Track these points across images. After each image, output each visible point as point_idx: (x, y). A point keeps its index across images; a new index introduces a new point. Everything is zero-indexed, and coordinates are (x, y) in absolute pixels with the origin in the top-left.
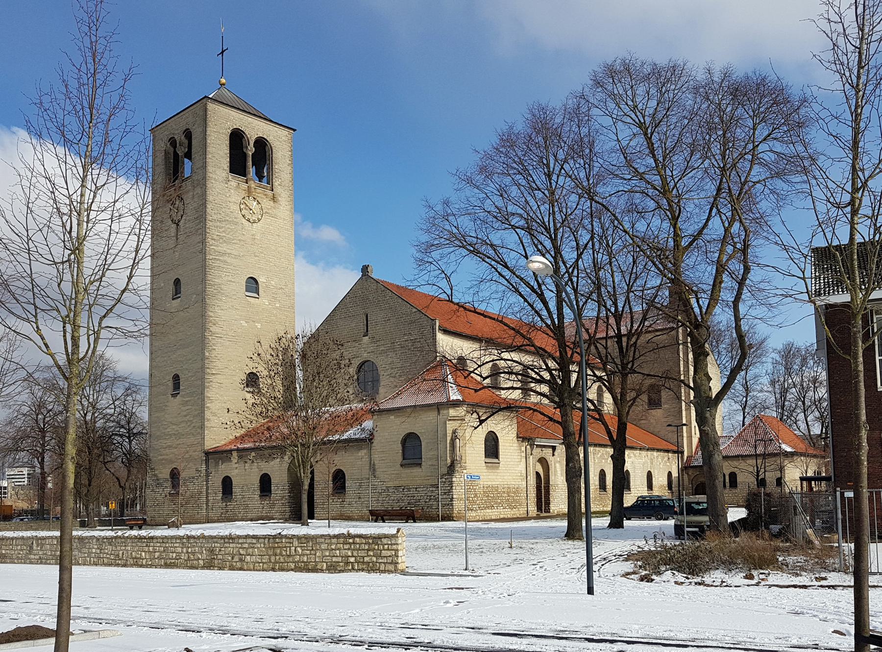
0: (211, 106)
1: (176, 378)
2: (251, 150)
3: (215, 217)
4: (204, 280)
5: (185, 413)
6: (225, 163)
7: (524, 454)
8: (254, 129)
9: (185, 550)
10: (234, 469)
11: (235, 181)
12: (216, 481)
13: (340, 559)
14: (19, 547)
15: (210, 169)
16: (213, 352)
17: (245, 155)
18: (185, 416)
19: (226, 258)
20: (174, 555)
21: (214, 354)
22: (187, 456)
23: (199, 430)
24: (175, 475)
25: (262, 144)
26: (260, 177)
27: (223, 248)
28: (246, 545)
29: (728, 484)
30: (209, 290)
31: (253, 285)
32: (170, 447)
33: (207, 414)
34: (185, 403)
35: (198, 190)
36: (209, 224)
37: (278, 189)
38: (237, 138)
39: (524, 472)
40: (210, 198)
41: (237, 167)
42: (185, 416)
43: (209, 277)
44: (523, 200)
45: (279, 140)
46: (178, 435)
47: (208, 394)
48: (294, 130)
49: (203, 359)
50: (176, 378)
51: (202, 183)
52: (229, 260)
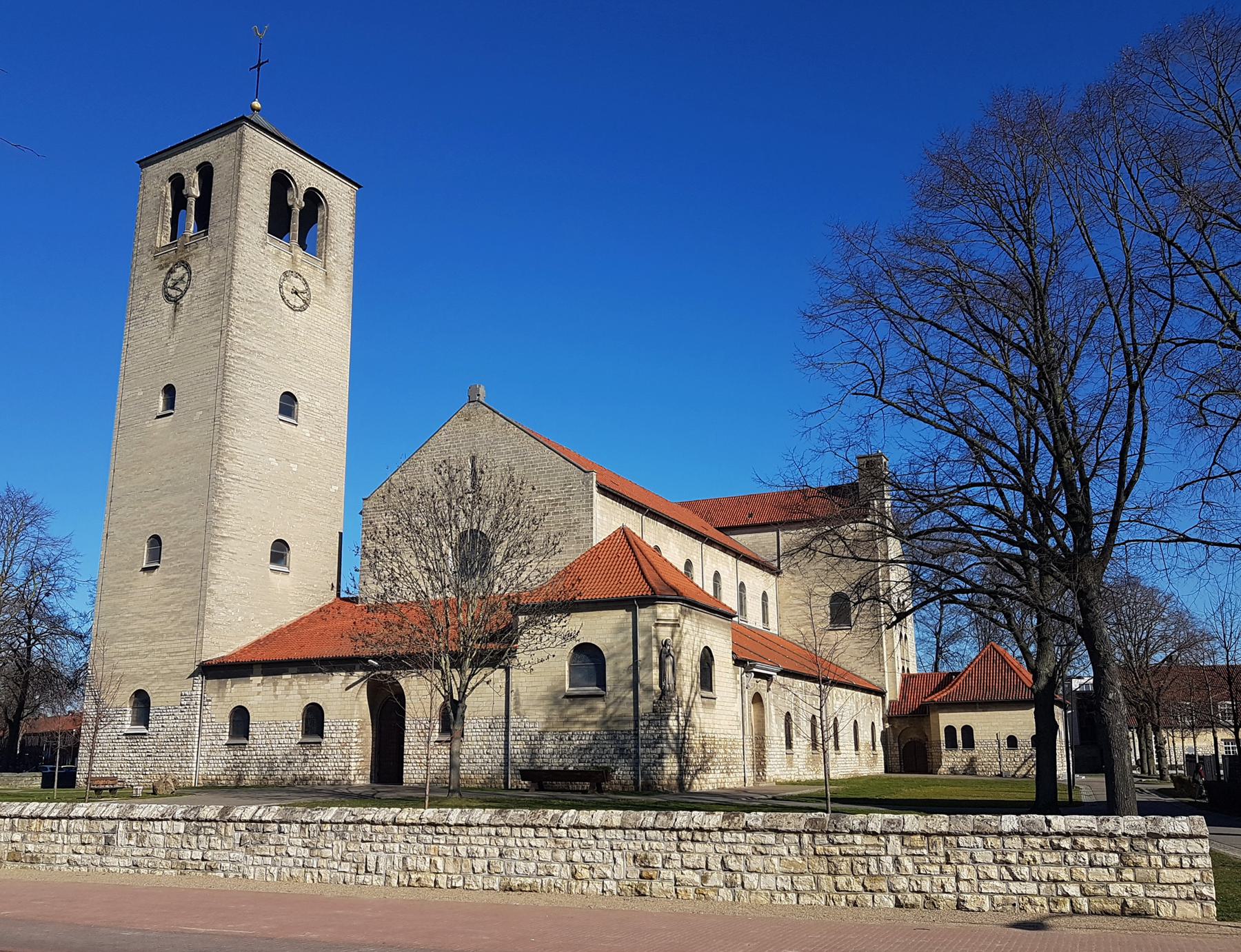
0: (249, 131)
1: (156, 541)
2: (297, 201)
3: (243, 295)
4: (221, 388)
5: (167, 600)
6: (263, 217)
7: (739, 687)
8: (307, 174)
9: (562, 855)
10: (252, 692)
11: (275, 245)
12: (220, 716)
13: (1032, 888)
14: (76, 839)
15: (242, 222)
16: (226, 502)
17: (290, 209)
18: (168, 604)
19: (254, 359)
20: (532, 867)
21: (226, 505)
22: (165, 670)
23: (192, 629)
24: (142, 701)
25: (314, 198)
26: (302, 244)
27: (252, 343)
28: (748, 850)
29: (960, 744)
30: (229, 404)
31: (288, 404)
32: (133, 654)
33: (211, 602)
34: (168, 584)
35: (220, 253)
36: (234, 303)
37: (333, 267)
38: (281, 181)
39: (740, 715)
40: (239, 265)
41: (278, 225)
42: (168, 604)
43: (229, 385)
44: (1196, 177)
45: (340, 199)
46: (152, 636)
47: (216, 569)
48: (359, 187)
49: (211, 511)
50: (156, 541)
51: (230, 244)
52: (259, 362)
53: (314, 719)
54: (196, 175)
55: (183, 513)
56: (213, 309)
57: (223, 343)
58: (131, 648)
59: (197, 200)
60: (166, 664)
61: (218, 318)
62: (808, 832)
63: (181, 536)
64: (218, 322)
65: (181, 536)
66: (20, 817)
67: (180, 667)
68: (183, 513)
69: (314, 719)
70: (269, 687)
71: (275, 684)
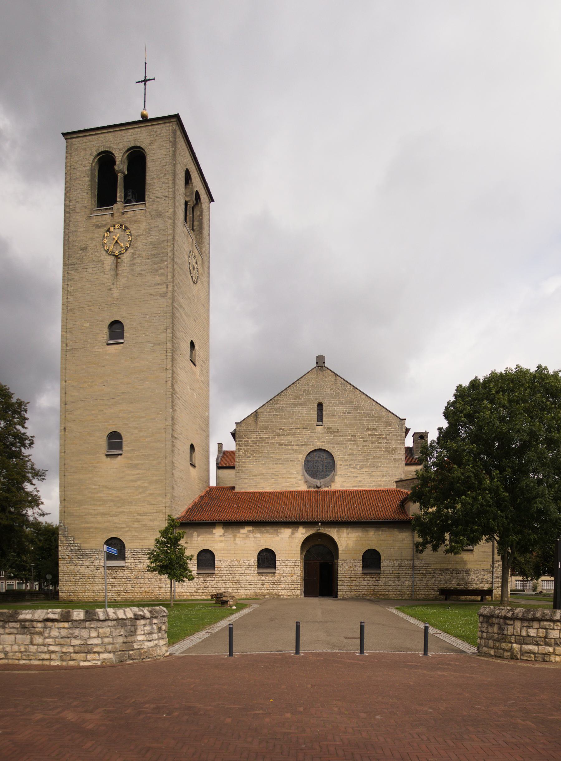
5: (133, 478)
32: (103, 514)
42: (132, 481)
53: (267, 560)
54: (118, 199)
55: (142, 417)
56: (156, 266)
57: (170, 295)
58: (101, 509)
59: (125, 177)
60: (138, 521)
61: (162, 274)
62: (523, 636)
63: (142, 434)
64: (163, 278)
65: (142, 434)
66: (173, 308)
67: (151, 523)
68: (142, 417)
69: (267, 560)
70: (229, 537)
71: (235, 536)
